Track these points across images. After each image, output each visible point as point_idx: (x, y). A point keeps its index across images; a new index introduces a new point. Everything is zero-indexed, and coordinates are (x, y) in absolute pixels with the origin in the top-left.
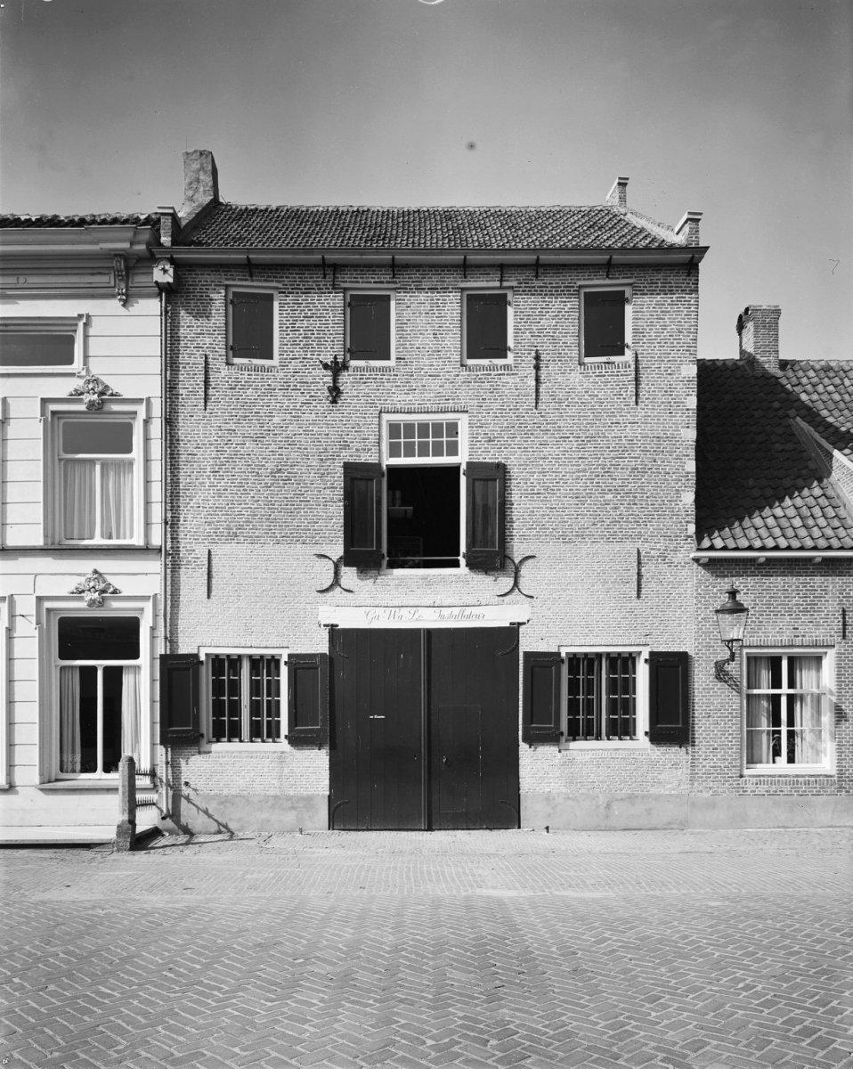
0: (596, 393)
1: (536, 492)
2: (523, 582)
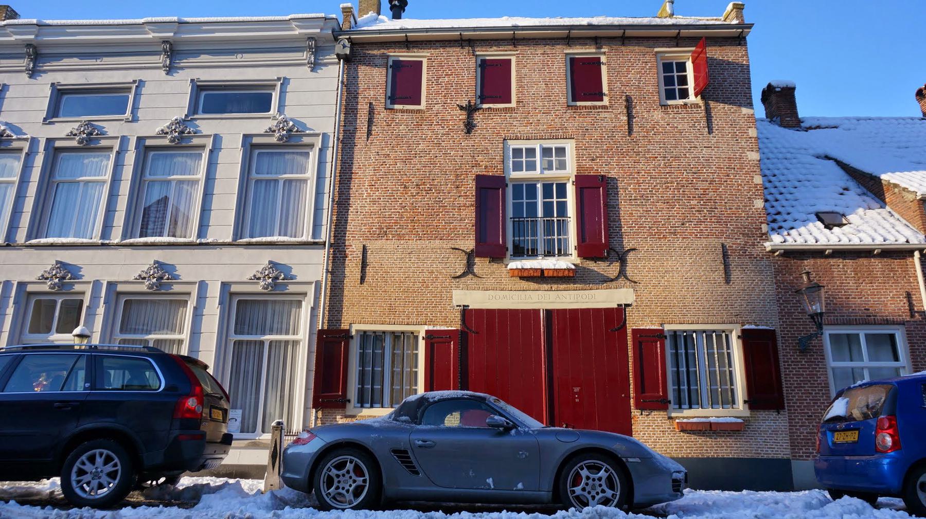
0: (676, 126)
1: (633, 198)
2: (629, 271)
